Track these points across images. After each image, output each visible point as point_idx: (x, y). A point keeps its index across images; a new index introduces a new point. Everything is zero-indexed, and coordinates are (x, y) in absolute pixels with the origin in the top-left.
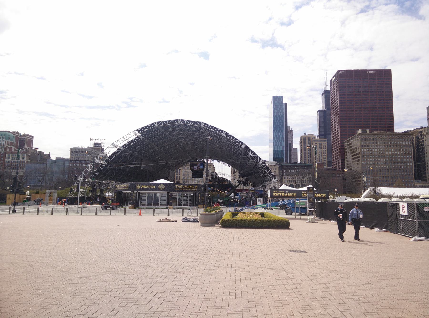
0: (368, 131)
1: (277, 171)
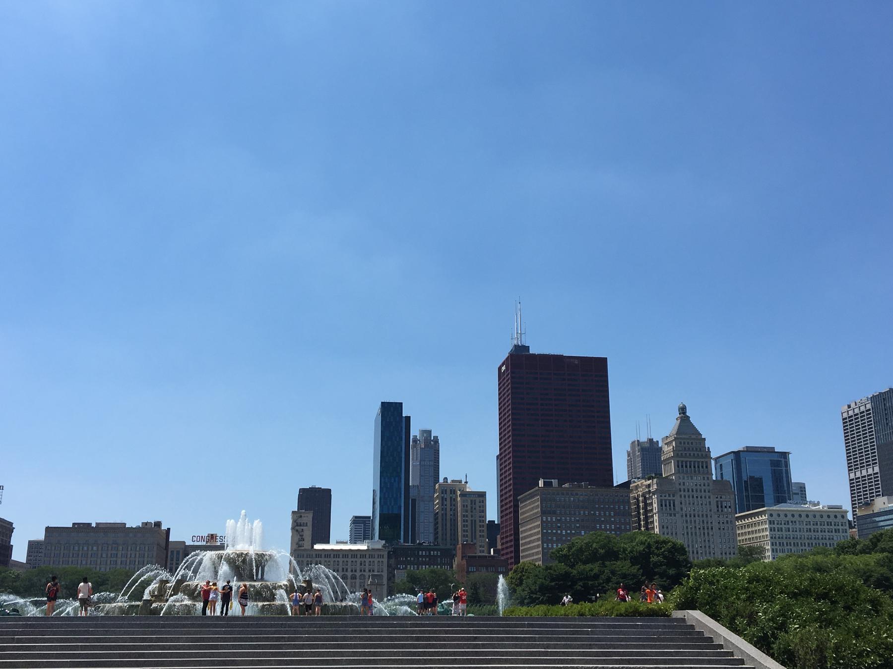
0: (555, 482)
1: (385, 560)
